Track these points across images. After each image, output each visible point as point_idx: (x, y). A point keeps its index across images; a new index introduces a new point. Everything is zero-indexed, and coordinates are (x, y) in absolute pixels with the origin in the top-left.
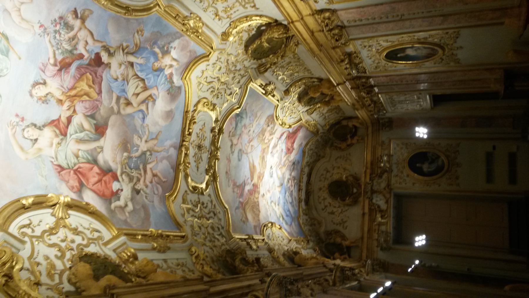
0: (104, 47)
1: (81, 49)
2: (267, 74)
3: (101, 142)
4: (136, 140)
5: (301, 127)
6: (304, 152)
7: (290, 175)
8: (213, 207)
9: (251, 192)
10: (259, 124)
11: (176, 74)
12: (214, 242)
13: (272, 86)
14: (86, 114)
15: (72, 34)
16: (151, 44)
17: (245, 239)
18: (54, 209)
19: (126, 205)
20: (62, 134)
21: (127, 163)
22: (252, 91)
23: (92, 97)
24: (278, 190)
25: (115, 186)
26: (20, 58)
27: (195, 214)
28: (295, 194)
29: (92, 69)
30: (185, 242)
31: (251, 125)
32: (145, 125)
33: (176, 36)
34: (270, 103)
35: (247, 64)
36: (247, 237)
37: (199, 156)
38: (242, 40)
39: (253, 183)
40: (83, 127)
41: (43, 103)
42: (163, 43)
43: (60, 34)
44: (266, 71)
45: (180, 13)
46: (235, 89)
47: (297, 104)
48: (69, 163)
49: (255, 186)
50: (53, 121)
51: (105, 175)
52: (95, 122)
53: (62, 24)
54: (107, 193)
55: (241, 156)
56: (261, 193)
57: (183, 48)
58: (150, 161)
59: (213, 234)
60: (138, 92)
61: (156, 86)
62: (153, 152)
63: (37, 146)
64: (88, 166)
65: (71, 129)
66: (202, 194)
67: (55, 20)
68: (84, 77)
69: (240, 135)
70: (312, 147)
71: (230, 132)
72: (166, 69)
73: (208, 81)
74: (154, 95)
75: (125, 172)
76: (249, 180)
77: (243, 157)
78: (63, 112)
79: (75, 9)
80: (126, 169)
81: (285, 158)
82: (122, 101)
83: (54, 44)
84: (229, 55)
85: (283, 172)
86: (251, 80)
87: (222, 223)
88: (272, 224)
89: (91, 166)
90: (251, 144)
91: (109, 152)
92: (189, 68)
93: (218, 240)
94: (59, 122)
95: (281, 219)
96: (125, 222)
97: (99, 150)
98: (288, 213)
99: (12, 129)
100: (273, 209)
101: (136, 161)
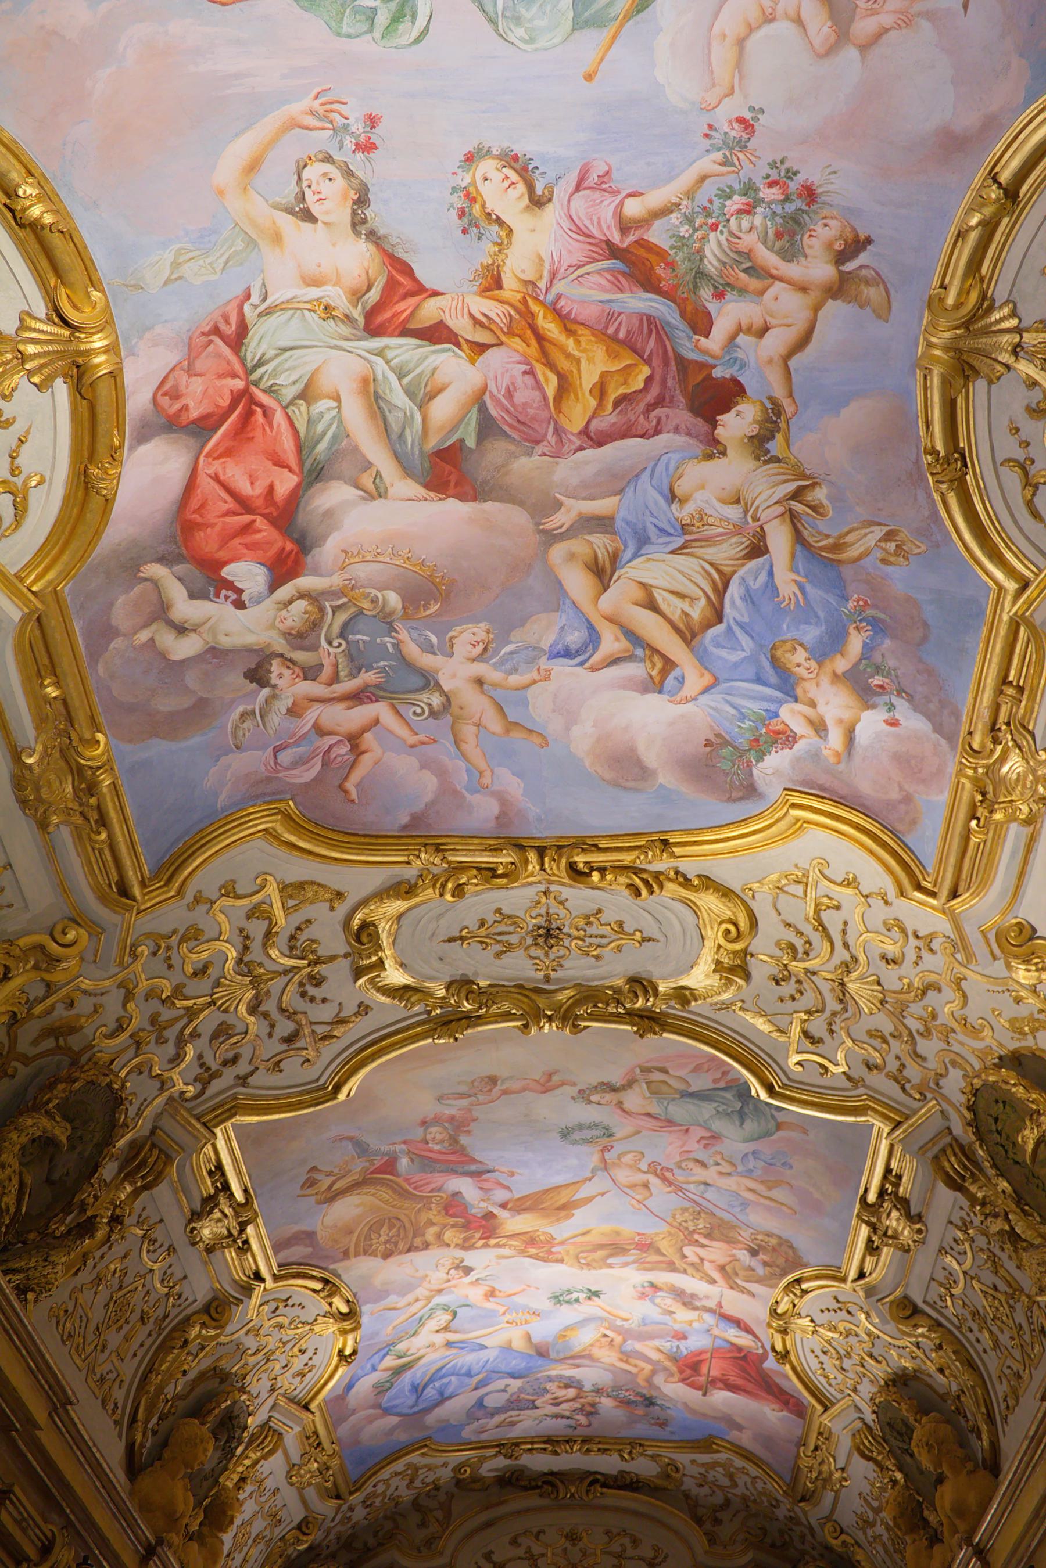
0: (777, 409)
1: (727, 314)
2: (945, 1196)
3: (404, 487)
4: (468, 636)
5: (799, 1410)
6: (706, 1444)
7: (598, 1391)
8: (321, 1030)
9: (454, 1206)
10: (745, 1204)
11: (798, 760)
12: (161, 1041)
13: (906, 1234)
14: (487, 398)
15: (768, 258)
16: (870, 612)
17: (226, 1187)
18: (49, 320)
19: (181, 630)
20: (370, 315)
21: (361, 612)
22: (856, 1144)
23: (564, 408)
24: (516, 1337)
25: (247, 573)
26: (589, 77)
27: (256, 945)
28: (527, 1424)
29: (670, 382)
30: (103, 899)
31: (726, 1168)
32: (544, 663)
33: (941, 713)
34: (842, 1244)
35: (954, 1084)
36: (239, 1196)
37: (514, 939)
38: (1033, 1031)
39: (496, 1211)
40: (432, 396)
41: (462, 213)
42: (891, 663)
43: (748, 211)
44: (955, 1185)
45: (1032, 698)
46: (840, 1056)
47: (879, 1371)
48: (269, 367)
49: (483, 1228)
50: (407, 270)
51: (273, 521)
52: (471, 443)
53: (790, 208)
54: (207, 542)
55: (589, 1142)
56: (471, 1258)
57: (907, 762)
58: (408, 712)
59: (195, 1035)
60: (663, 606)
61: (716, 682)
62: (449, 718)
63: (287, 223)
64: (288, 444)
65: (404, 349)
66: (358, 972)
67: (791, 174)
68: (628, 359)
69: (670, 1122)
70: (741, 1479)
71: (664, 1071)
72: (798, 707)
73: (825, 916)
74: (681, 680)
75: (322, 610)
76: (501, 1195)
77: (584, 1149)
78: (457, 303)
79: (869, 241)
80: (335, 609)
81: (655, 1356)
82: (601, 543)
83: (702, 198)
84: (958, 983)
85: (597, 1352)
86: (899, 1124)
87: (261, 1078)
88: (344, 1317)
89: (292, 460)
90: (653, 1180)
91: (378, 526)
92: (840, 812)
93: (177, 1059)
94: (413, 294)
95: (390, 1362)
96: (109, 632)
97: (367, 480)
98: (430, 1392)
99: (312, 113)
100: (421, 1322)
101: (384, 654)
